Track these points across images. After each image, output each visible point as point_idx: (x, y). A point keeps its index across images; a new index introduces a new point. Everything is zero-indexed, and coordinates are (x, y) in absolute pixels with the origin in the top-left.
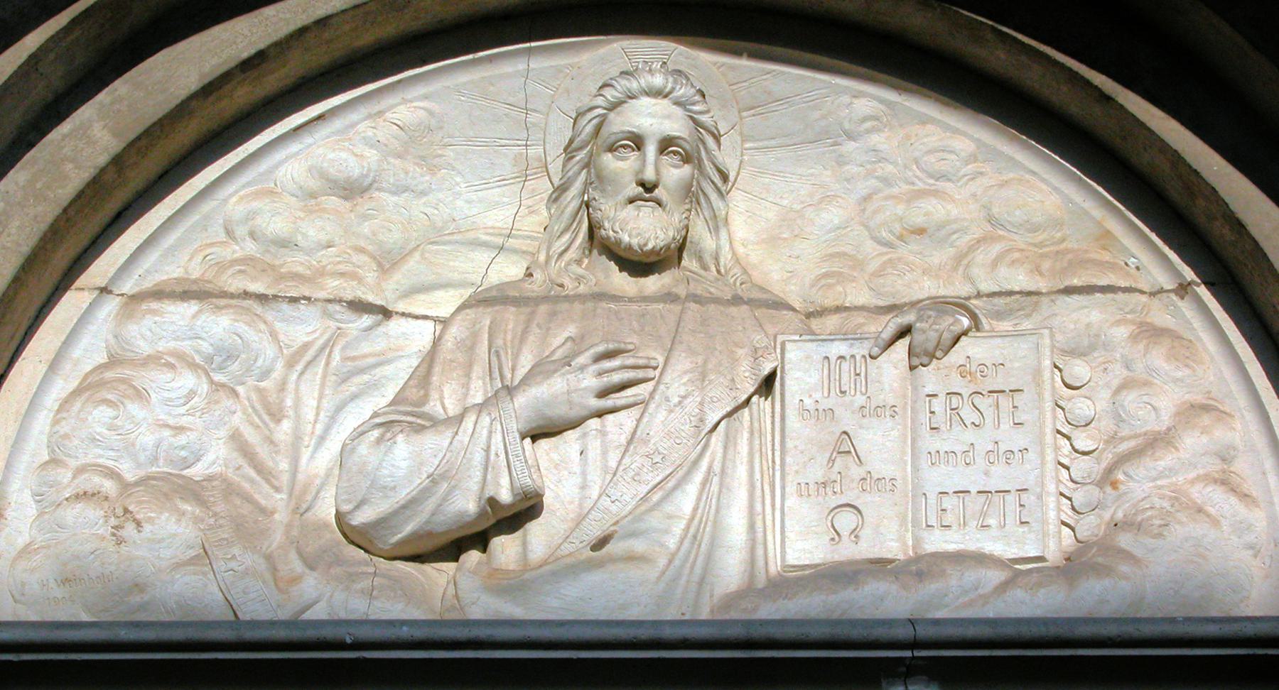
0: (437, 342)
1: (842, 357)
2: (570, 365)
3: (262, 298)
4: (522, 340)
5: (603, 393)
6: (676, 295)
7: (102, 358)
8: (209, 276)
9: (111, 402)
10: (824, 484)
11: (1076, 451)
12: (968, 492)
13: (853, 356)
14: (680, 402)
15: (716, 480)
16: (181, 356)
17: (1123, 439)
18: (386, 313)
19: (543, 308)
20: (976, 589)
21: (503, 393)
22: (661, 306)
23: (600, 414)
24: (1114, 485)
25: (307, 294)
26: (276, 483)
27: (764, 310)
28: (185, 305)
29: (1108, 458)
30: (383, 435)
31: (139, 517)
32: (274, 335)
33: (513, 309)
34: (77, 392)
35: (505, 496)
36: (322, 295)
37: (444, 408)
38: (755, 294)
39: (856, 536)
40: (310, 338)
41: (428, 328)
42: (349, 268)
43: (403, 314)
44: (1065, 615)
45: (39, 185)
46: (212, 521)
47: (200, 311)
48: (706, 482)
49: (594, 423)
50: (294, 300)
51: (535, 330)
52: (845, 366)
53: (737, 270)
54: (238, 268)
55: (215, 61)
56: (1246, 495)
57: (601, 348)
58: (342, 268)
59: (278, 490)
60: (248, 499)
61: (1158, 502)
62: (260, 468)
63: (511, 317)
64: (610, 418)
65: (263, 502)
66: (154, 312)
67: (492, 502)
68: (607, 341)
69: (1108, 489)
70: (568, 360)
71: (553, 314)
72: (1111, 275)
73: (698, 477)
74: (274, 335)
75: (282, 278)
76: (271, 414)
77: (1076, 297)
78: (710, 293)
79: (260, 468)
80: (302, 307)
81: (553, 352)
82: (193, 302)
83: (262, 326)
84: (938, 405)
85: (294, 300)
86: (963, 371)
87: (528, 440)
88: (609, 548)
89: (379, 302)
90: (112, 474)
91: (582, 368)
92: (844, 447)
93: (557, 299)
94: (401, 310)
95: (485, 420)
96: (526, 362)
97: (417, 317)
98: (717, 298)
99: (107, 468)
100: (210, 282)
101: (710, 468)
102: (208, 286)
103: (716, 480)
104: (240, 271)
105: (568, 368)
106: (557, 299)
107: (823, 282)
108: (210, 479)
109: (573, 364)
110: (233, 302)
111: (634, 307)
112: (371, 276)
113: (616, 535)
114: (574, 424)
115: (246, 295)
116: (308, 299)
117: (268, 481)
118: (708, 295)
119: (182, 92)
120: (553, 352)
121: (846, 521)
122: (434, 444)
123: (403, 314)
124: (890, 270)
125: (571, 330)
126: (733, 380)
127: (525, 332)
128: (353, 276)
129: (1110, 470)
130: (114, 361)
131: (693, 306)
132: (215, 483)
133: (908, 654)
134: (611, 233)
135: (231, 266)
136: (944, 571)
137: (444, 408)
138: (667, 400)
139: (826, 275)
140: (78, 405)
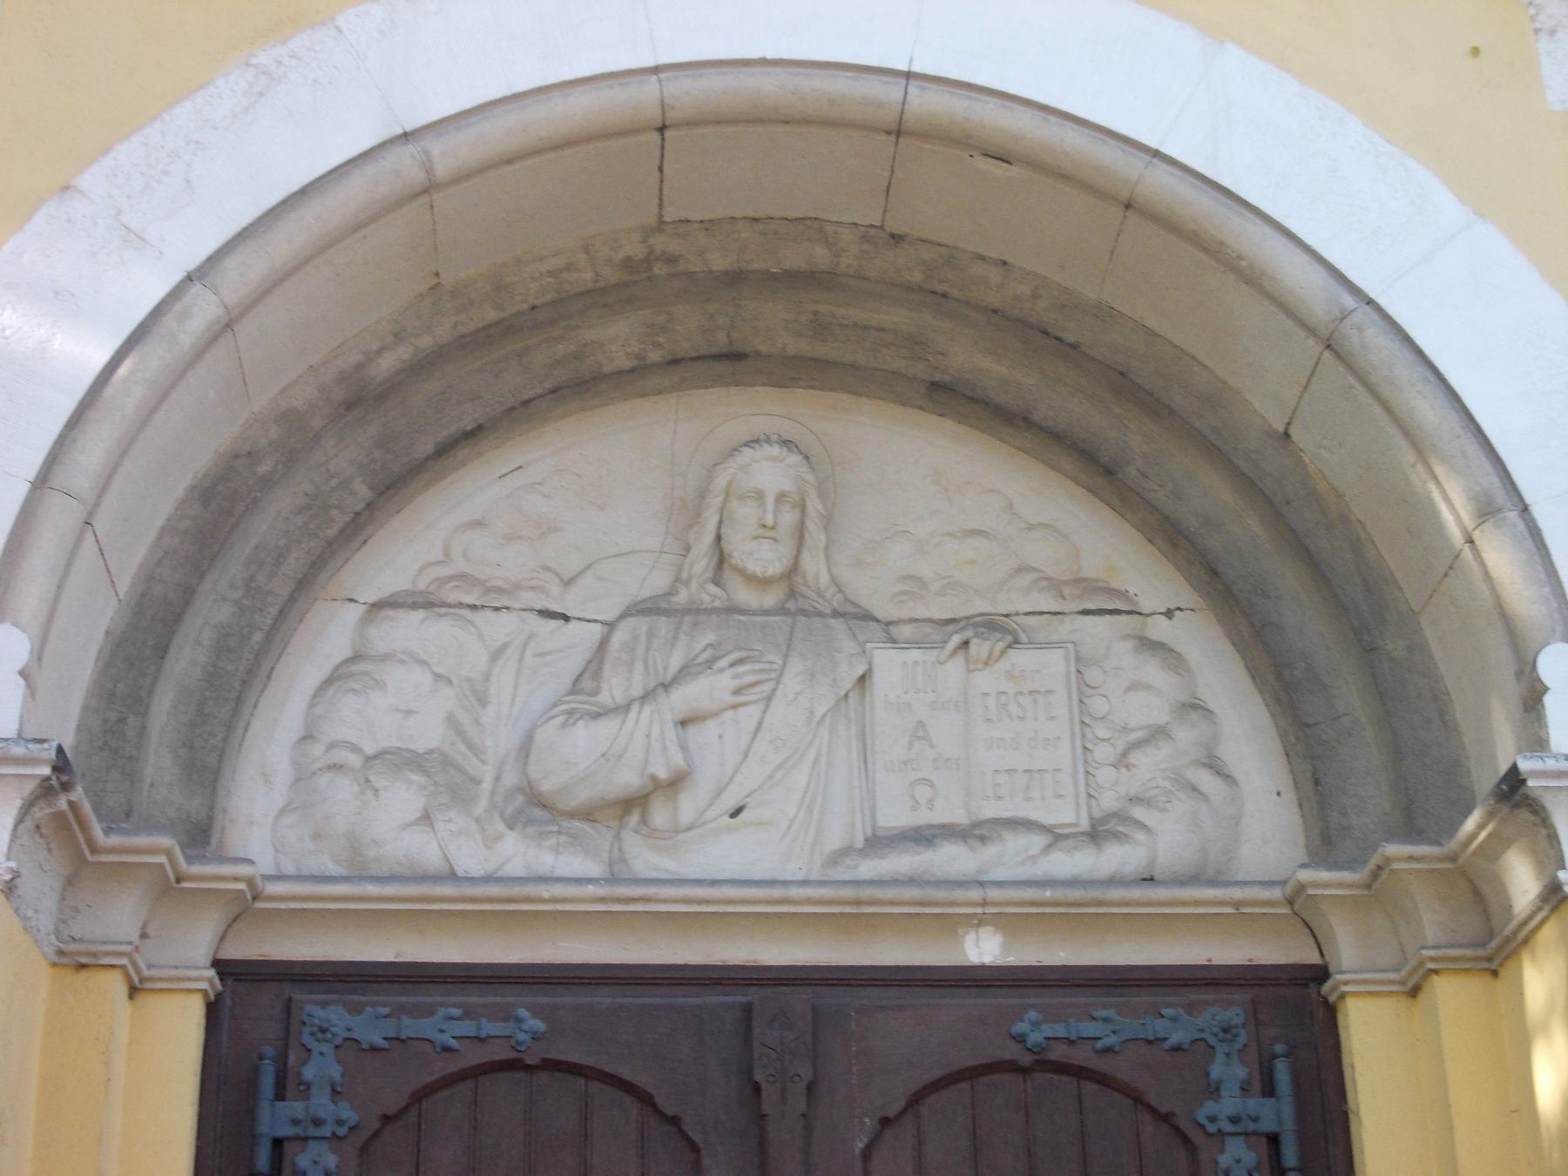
0: (603, 644)
1: (916, 663)
2: (711, 669)
3: (473, 607)
4: (673, 645)
5: (737, 692)
6: (788, 609)
7: (346, 653)
8: (432, 589)
9: (357, 691)
10: (905, 763)
11: (1097, 738)
12: (1016, 770)
13: (925, 662)
14: (795, 699)
15: (824, 759)
16: (412, 655)
17: (1132, 730)
18: (566, 618)
19: (689, 619)
20: (1026, 851)
21: (660, 690)
22: (777, 618)
23: (735, 707)
24: (1128, 767)
25: (506, 604)
26: (482, 757)
27: (855, 622)
28: (415, 612)
29: (1121, 745)
30: (567, 720)
31: (377, 785)
32: (481, 636)
33: (664, 618)
34: (328, 682)
35: (662, 774)
36: (518, 605)
37: (613, 698)
38: (850, 609)
39: (931, 801)
40: (508, 639)
41: (597, 628)
42: (540, 583)
43: (579, 619)
44: (963, 428)
45: (312, 526)
46: (433, 788)
47: (426, 619)
48: (816, 762)
49: (729, 714)
50: (497, 609)
51: (682, 637)
52: (919, 669)
53: (833, 589)
54: (456, 583)
55: (446, 433)
56: (1228, 776)
57: (735, 656)
58: (534, 583)
59: (483, 762)
60: (460, 770)
61: (1162, 783)
62: (471, 746)
63: (664, 625)
64: (742, 710)
65: (471, 772)
66: (389, 618)
67: (653, 778)
68: (739, 649)
69: (1123, 770)
70: (708, 664)
71: (695, 625)
72: (1118, 602)
73: (811, 756)
74: (481, 636)
75: (490, 590)
76: (479, 700)
77: (1090, 617)
78: (815, 608)
79: (471, 746)
80: (504, 615)
81: (697, 655)
82: (421, 610)
83: (473, 630)
84: (991, 701)
85: (497, 609)
86: (1010, 676)
87: (679, 727)
88: (742, 816)
89: (560, 610)
90: (356, 749)
91: (721, 671)
92: (920, 733)
93: (699, 611)
94: (576, 616)
95: (647, 710)
96: (676, 661)
97: (589, 621)
98: (819, 612)
99: (352, 744)
100: (432, 594)
101: (818, 755)
102: (431, 596)
103: (824, 759)
104: (457, 586)
105: (710, 671)
106: (699, 611)
107: (898, 598)
108: (431, 752)
109: (714, 667)
110: (452, 610)
111: (758, 619)
112: (555, 589)
113: (748, 806)
114: (715, 714)
115: (461, 605)
116: (507, 608)
117: (476, 755)
118: (812, 609)
119: (422, 456)
120: (697, 655)
121: (923, 792)
122: (606, 729)
123: (579, 619)
124: (949, 591)
125: (710, 638)
126: (834, 680)
127: (675, 638)
128: (543, 590)
129: (1125, 754)
130: (356, 658)
131: (803, 619)
132: (435, 756)
133: (979, 910)
134: (738, 561)
135: (449, 582)
136: (1000, 836)
137: (613, 698)
138: (786, 696)
139: (902, 593)
140: (331, 692)
